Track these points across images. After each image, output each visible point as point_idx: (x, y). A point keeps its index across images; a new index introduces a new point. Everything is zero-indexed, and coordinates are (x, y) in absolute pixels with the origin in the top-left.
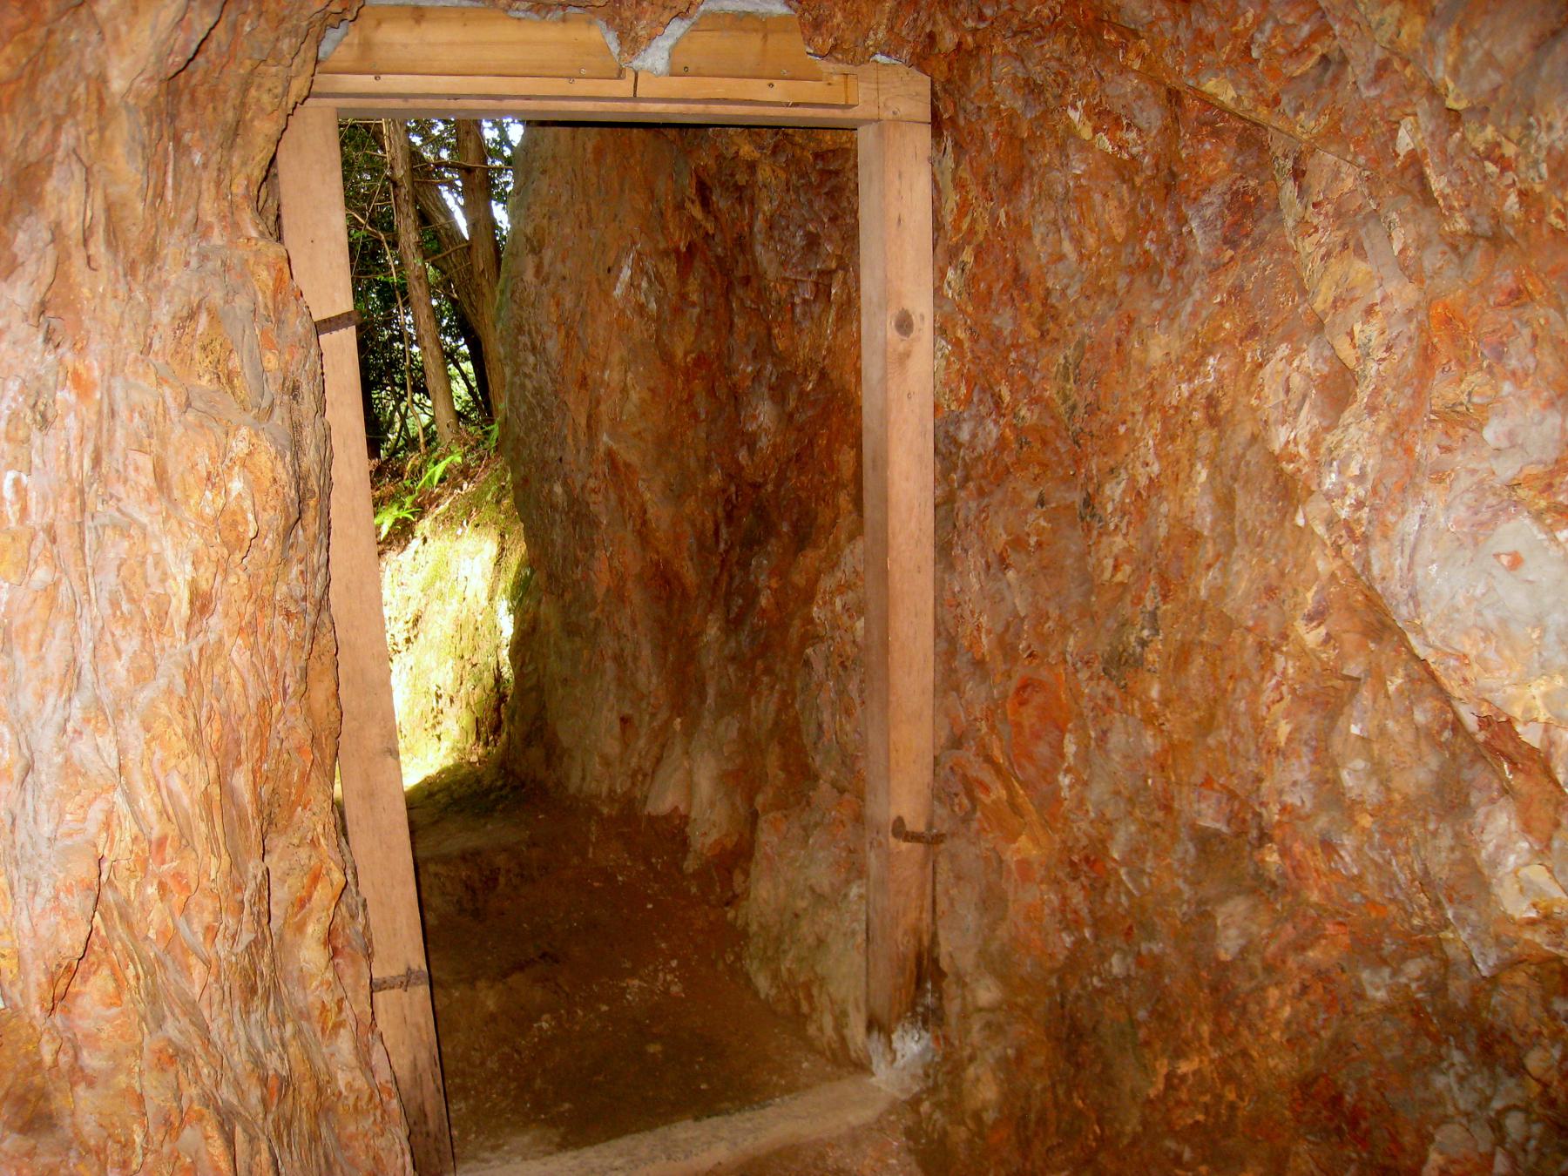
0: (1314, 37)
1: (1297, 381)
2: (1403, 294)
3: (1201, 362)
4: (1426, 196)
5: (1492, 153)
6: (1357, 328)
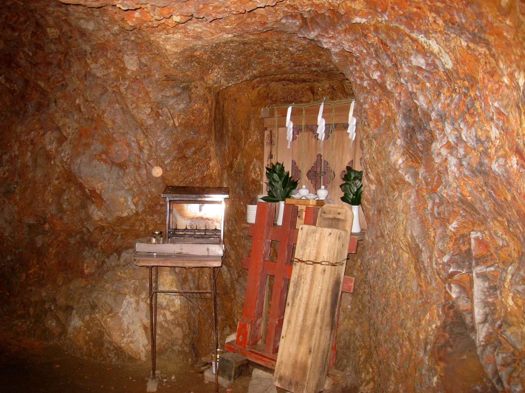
0: (62, 81)
1: (52, 138)
2: (76, 125)
3: (30, 132)
4: (80, 111)
5: (94, 108)
6: (67, 130)
